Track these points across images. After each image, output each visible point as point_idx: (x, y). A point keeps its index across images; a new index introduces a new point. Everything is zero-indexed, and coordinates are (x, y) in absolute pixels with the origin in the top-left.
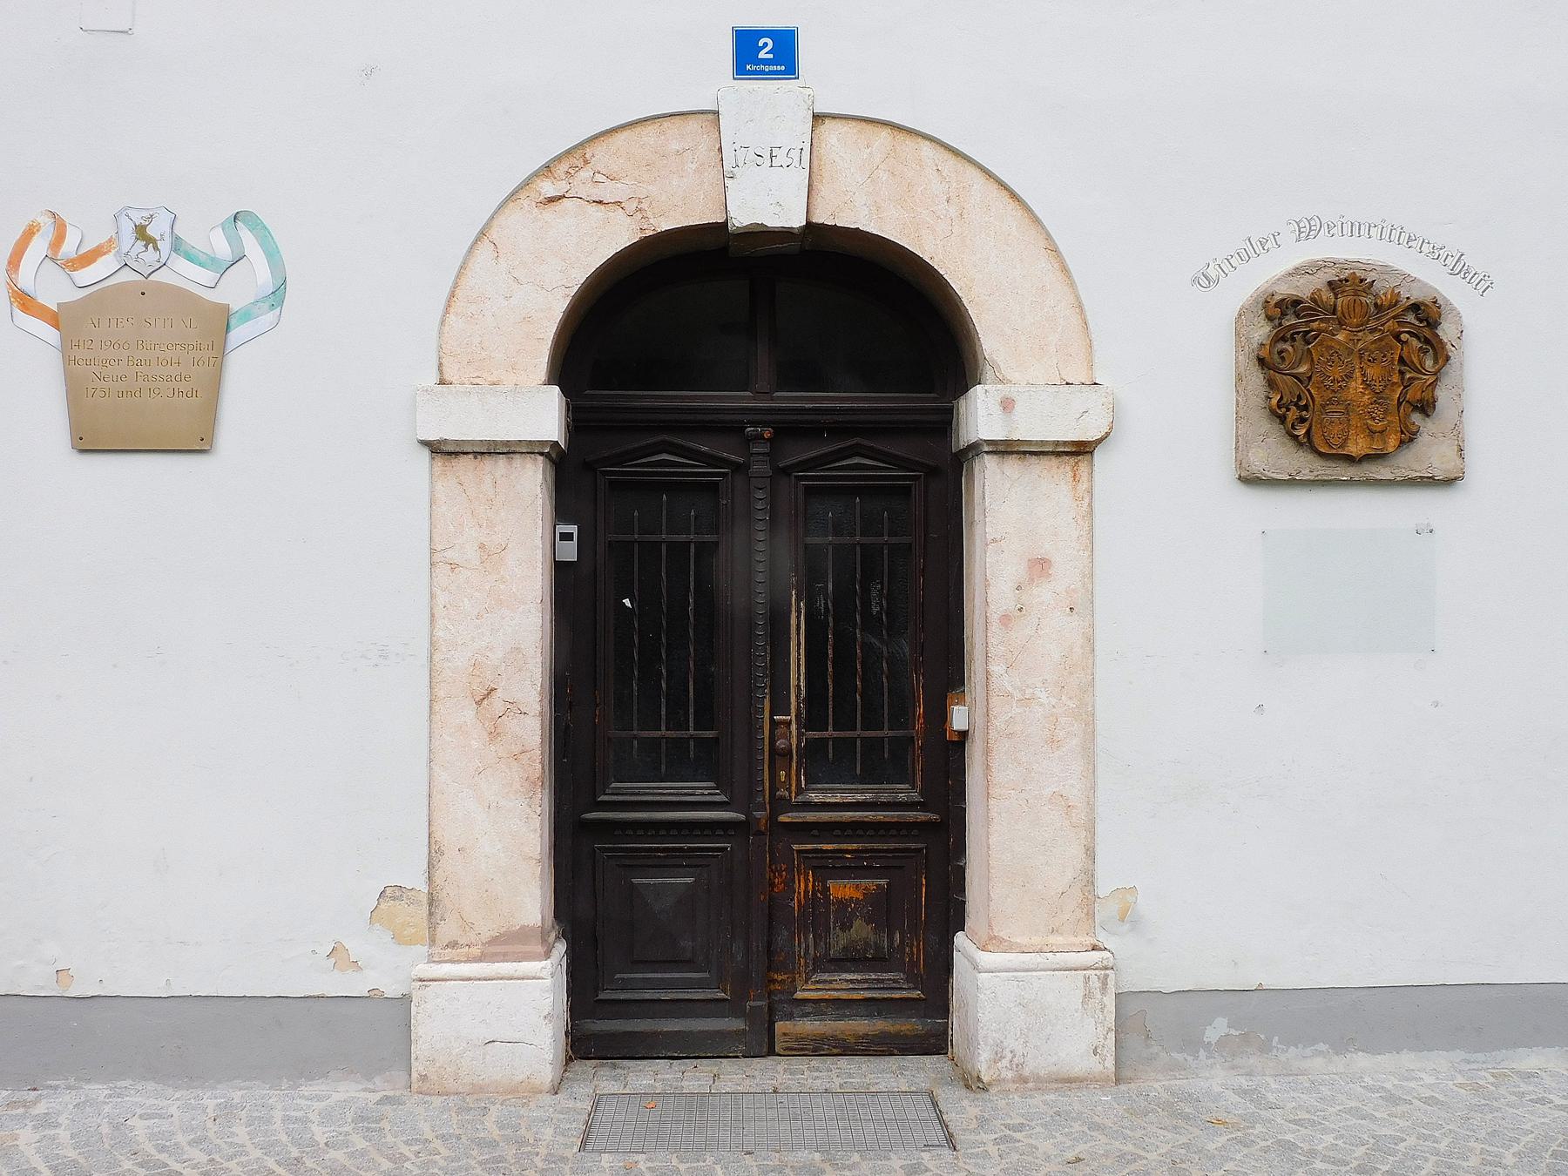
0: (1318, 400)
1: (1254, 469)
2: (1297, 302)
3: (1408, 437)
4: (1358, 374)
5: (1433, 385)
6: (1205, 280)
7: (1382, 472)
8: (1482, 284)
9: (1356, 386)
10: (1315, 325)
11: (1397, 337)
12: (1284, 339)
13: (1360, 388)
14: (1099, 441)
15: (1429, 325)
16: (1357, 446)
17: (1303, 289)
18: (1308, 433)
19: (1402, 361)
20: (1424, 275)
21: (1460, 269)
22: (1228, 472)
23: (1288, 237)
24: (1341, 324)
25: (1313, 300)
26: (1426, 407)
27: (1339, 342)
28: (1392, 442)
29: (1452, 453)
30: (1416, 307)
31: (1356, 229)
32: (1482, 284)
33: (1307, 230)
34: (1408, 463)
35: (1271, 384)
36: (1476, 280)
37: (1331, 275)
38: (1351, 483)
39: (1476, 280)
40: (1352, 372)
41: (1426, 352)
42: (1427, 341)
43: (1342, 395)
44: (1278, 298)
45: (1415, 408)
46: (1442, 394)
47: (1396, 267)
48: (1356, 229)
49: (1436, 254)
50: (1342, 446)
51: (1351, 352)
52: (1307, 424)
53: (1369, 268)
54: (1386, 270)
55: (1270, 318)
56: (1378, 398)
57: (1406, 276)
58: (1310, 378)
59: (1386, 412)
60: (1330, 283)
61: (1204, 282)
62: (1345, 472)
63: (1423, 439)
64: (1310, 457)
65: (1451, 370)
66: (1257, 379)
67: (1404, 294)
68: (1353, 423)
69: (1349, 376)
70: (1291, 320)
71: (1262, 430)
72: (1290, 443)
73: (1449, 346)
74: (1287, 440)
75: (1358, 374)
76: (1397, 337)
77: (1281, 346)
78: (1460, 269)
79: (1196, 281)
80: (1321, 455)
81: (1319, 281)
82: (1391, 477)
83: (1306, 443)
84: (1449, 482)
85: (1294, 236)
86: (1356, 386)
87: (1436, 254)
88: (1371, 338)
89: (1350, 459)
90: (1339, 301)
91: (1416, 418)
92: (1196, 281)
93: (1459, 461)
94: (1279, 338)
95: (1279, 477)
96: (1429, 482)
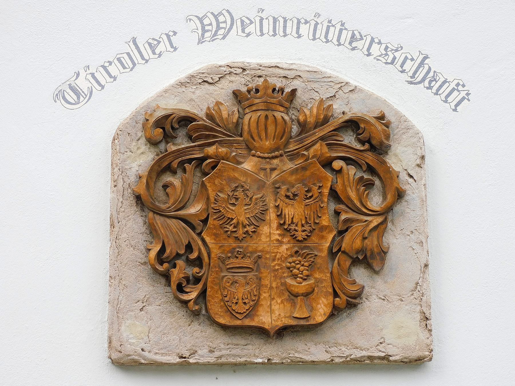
0: (215, 251)
1: (128, 349)
2: (186, 120)
3: (347, 303)
4: (272, 215)
5: (381, 229)
6: (71, 95)
7: (313, 350)
8: (455, 95)
9: (270, 231)
10: (211, 150)
11: (327, 164)
12: (169, 169)
13: (276, 234)
14: (374, 270)
15: (373, 148)
16: (270, 316)
17: (197, 103)
18: (203, 294)
19: (334, 194)
20: (368, 83)
21: (422, 75)
22: (100, 353)
23: (187, 37)
24: (249, 149)
25: (210, 116)
26: (371, 259)
27: (245, 173)
28: (322, 309)
29: (413, 323)
30: (353, 124)
31: (279, 26)
32: (455, 95)
33: (213, 27)
34: (353, 336)
35: (152, 231)
36: (446, 90)
37: (239, 83)
38: (269, 366)
39: (446, 90)
40: (264, 212)
41: (369, 185)
42: (371, 170)
43: (251, 244)
44: (159, 114)
45: (356, 262)
46: (397, 242)
47: (329, 72)
48: (279, 26)
49: (391, 56)
50: (251, 313)
51: (262, 186)
52: (200, 286)
53: (291, 74)
54: (316, 76)
55: (153, 143)
56: (302, 246)
57: (343, 85)
58: (205, 221)
59: (312, 266)
60: (236, 94)
61: (71, 96)
62: (258, 351)
63: (371, 304)
64: (209, 331)
65: (408, 211)
66: (135, 223)
67: (338, 107)
68: (266, 282)
69: (260, 218)
70: (182, 143)
71: (141, 295)
72: (180, 314)
73: (404, 176)
74: (175, 307)
75: (272, 215)
76: (327, 164)
77: (168, 178)
78: (422, 75)
79: (60, 95)
80: (224, 328)
81: (222, 93)
82: (326, 357)
83: (197, 311)
84: (415, 363)
85: (195, 38)
86: (270, 231)
87: (391, 56)
88: (290, 165)
89: (261, 332)
90: (247, 118)
91: (360, 275)
92: (60, 95)
93: (423, 335)
94: (161, 168)
95: (159, 358)
96: (383, 364)
